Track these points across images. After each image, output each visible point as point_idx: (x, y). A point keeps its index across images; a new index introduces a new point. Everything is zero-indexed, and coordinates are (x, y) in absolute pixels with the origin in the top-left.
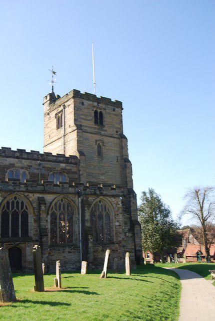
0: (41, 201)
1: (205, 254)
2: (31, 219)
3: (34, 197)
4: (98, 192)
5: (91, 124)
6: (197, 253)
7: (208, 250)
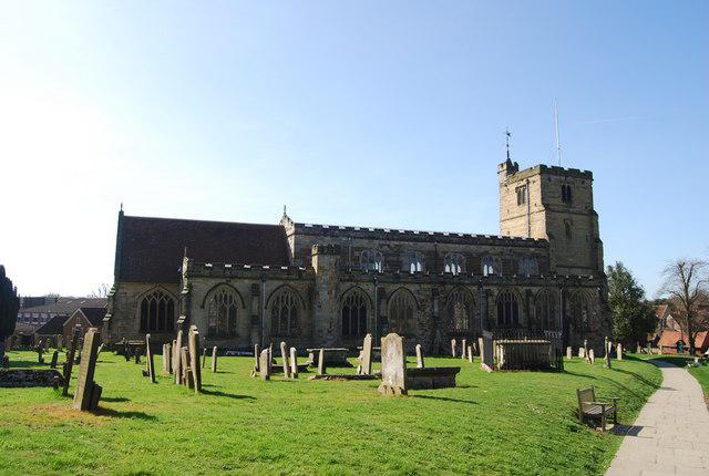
0: (529, 293)
1: (688, 345)
2: (520, 309)
3: (523, 289)
4: (577, 283)
5: (559, 201)
6: (678, 343)
7: (692, 341)
